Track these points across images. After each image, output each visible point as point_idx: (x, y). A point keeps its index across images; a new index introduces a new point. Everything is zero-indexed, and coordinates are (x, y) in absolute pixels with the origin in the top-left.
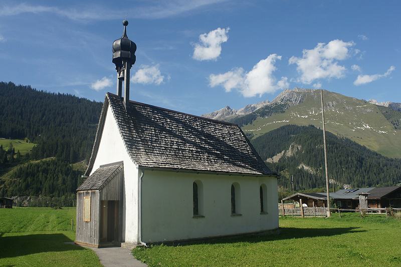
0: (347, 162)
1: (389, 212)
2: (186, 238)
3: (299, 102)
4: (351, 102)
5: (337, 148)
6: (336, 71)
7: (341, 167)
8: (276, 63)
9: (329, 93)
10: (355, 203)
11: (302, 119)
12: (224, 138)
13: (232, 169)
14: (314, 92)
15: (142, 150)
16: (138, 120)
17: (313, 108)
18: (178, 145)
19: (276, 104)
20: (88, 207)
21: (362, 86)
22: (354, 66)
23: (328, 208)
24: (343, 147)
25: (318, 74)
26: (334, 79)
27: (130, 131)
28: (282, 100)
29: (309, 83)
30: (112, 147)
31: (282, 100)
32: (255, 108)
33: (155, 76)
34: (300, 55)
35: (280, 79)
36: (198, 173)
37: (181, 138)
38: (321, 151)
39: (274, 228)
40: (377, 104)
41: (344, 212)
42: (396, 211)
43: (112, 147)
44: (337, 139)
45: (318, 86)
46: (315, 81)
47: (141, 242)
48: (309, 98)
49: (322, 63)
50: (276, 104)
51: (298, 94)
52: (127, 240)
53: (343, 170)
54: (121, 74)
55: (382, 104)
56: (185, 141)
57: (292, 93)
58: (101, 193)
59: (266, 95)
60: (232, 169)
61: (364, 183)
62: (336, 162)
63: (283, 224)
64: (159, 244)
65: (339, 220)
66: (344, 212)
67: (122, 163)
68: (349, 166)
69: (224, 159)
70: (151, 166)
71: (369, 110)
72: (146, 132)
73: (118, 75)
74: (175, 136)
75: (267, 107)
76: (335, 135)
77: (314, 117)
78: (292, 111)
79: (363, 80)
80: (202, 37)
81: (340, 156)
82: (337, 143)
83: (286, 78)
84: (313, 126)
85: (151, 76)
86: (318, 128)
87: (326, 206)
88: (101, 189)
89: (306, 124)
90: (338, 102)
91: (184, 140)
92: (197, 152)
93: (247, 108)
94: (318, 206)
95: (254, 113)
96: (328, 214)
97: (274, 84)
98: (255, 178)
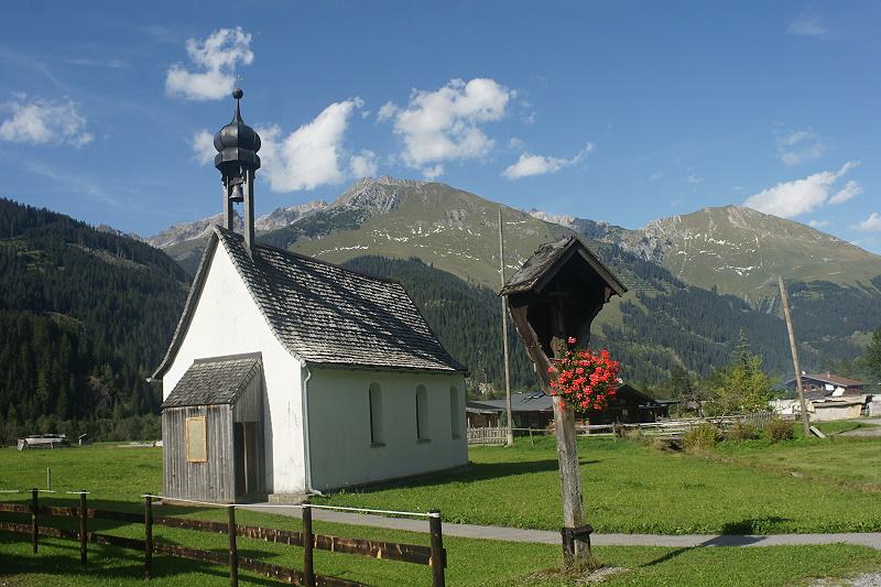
0: (487, 338)
1: (618, 431)
2: (364, 482)
3: (389, 206)
4: (493, 210)
5: (467, 309)
6: (475, 143)
7: (475, 347)
8: (353, 119)
9: (453, 191)
10: (545, 418)
11: (397, 243)
12: (388, 307)
13: (415, 363)
14: (423, 188)
15: (294, 333)
16: (273, 271)
17: (420, 223)
18: (336, 322)
19: (341, 209)
20: (199, 440)
21: (526, 181)
22: (513, 141)
23: (509, 428)
24: (478, 306)
25: (440, 149)
26: (471, 164)
27: (268, 298)
28: (355, 201)
29: (417, 167)
30: (227, 320)
31: (355, 201)
32: (294, 215)
33: (72, 129)
34: (403, 103)
35: (357, 153)
36: (402, 372)
37: (334, 308)
38: (434, 314)
39: (464, 462)
40: (545, 219)
41: (601, 431)
42: (630, 428)
43: (227, 320)
44: (466, 288)
45: (430, 176)
46: (432, 164)
47: (311, 490)
48: (414, 199)
49: (443, 125)
50: (341, 209)
51: (390, 189)
52: (277, 488)
53: (478, 354)
54: (235, 190)
55: (554, 220)
56: (343, 316)
57: (376, 188)
58: (234, 410)
59: (322, 189)
60: (415, 363)
61: (519, 380)
62: (465, 337)
63: (475, 457)
64: (338, 491)
65: (531, 449)
66: (601, 431)
67: (259, 355)
68: (490, 345)
69: (399, 346)
70: (319, 361)
71: (530, 232)
72: (288, 299)
73: (226, 191)
74: (327, 306)
75: (321, 215)
76: (462, 281)
77: (422, 240)
78: (374, 226)
79: (529, 166)
80: (191, 48)
81: (473, 325)
82: (466, 297)
83: (372, 154)
84: (418, 260)
85: (59, 129)
86: (429, 265)
87: (506, 425)
88: (233, 403)
89: (404, 255)
90: (470, 211)
91: (339, 312)
92: (363, 334)
93: (276, 214)
94: (476, 427)
95: (292, 226)
96: (509, 438)
97: (343, 164)
98: (349, 372)
